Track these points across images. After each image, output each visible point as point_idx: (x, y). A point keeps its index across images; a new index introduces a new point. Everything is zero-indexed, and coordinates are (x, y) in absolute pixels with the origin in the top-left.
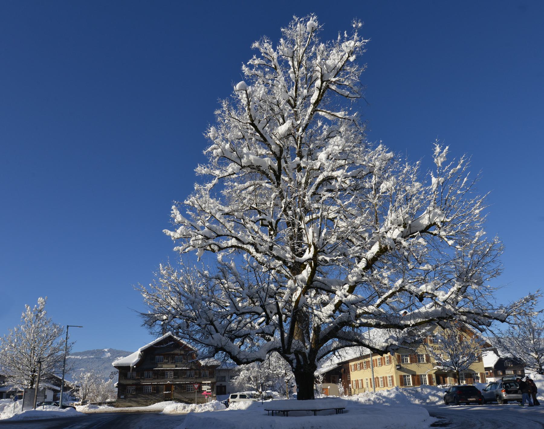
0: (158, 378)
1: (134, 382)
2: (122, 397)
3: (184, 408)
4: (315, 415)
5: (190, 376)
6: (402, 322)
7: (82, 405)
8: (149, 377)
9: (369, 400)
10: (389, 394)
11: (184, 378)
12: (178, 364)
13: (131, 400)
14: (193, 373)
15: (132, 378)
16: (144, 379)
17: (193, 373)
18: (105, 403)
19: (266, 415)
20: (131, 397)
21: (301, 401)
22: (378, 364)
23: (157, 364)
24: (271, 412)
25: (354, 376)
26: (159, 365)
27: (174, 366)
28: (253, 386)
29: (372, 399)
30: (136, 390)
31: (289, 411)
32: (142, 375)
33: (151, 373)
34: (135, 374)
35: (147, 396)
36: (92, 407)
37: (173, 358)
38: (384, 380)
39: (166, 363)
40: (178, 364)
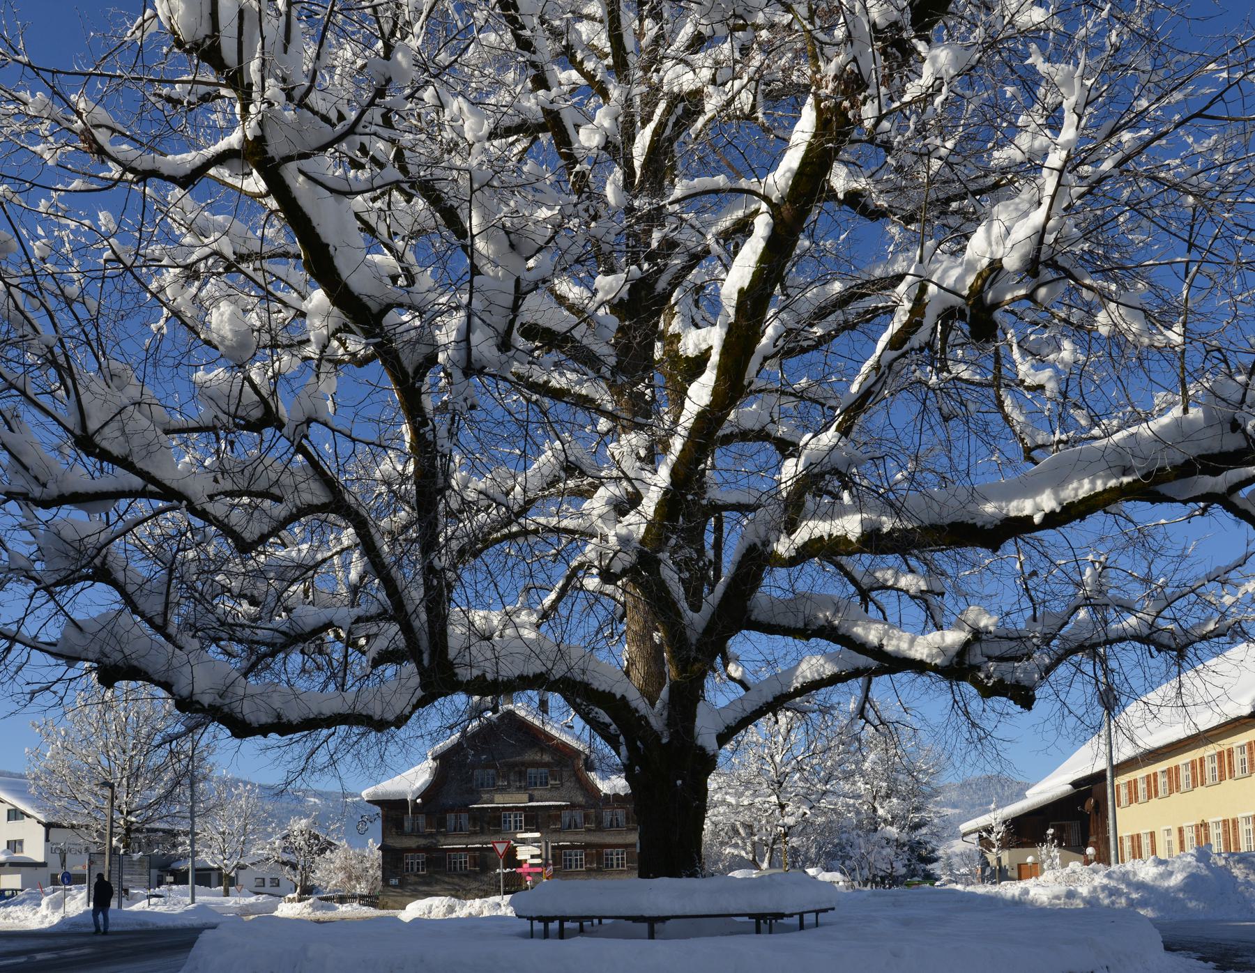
0: (482, 832)
1: (422, 842)
2: (394, 881)
3: (451, 909)
4: (652, 936)
5: (572, 826)
6: (989, 508)
7: (300, 901)
8: (458, 829)
9: (1071, 895)
10: (1163, 876)
11: (555, 831)
12: (536, 793)
13: (416, 890)
14: (578, 815)
15: (415, 832)
16: (445, 835)
17: (578, 815)
18: (353, 897)
19: (532, 935)
20: (416, 883)
21: (664, 881)
22: (1208, 774)
23: (478, 792)
24: (554, 926)
25: (1128, 820)
26: (485, 796)
27: (526, 797)
28: (743, 853)
29: (1084, 891)
30: (428, 863)
31: (664, 919)
32: (442, 823)
33: (464, 818)
34: (422, 820)
35: (456, 880)
36: (322, 908)
37: (521, 775)
38: (1226, 832)
39: (502, 790)
40: (536, 793)
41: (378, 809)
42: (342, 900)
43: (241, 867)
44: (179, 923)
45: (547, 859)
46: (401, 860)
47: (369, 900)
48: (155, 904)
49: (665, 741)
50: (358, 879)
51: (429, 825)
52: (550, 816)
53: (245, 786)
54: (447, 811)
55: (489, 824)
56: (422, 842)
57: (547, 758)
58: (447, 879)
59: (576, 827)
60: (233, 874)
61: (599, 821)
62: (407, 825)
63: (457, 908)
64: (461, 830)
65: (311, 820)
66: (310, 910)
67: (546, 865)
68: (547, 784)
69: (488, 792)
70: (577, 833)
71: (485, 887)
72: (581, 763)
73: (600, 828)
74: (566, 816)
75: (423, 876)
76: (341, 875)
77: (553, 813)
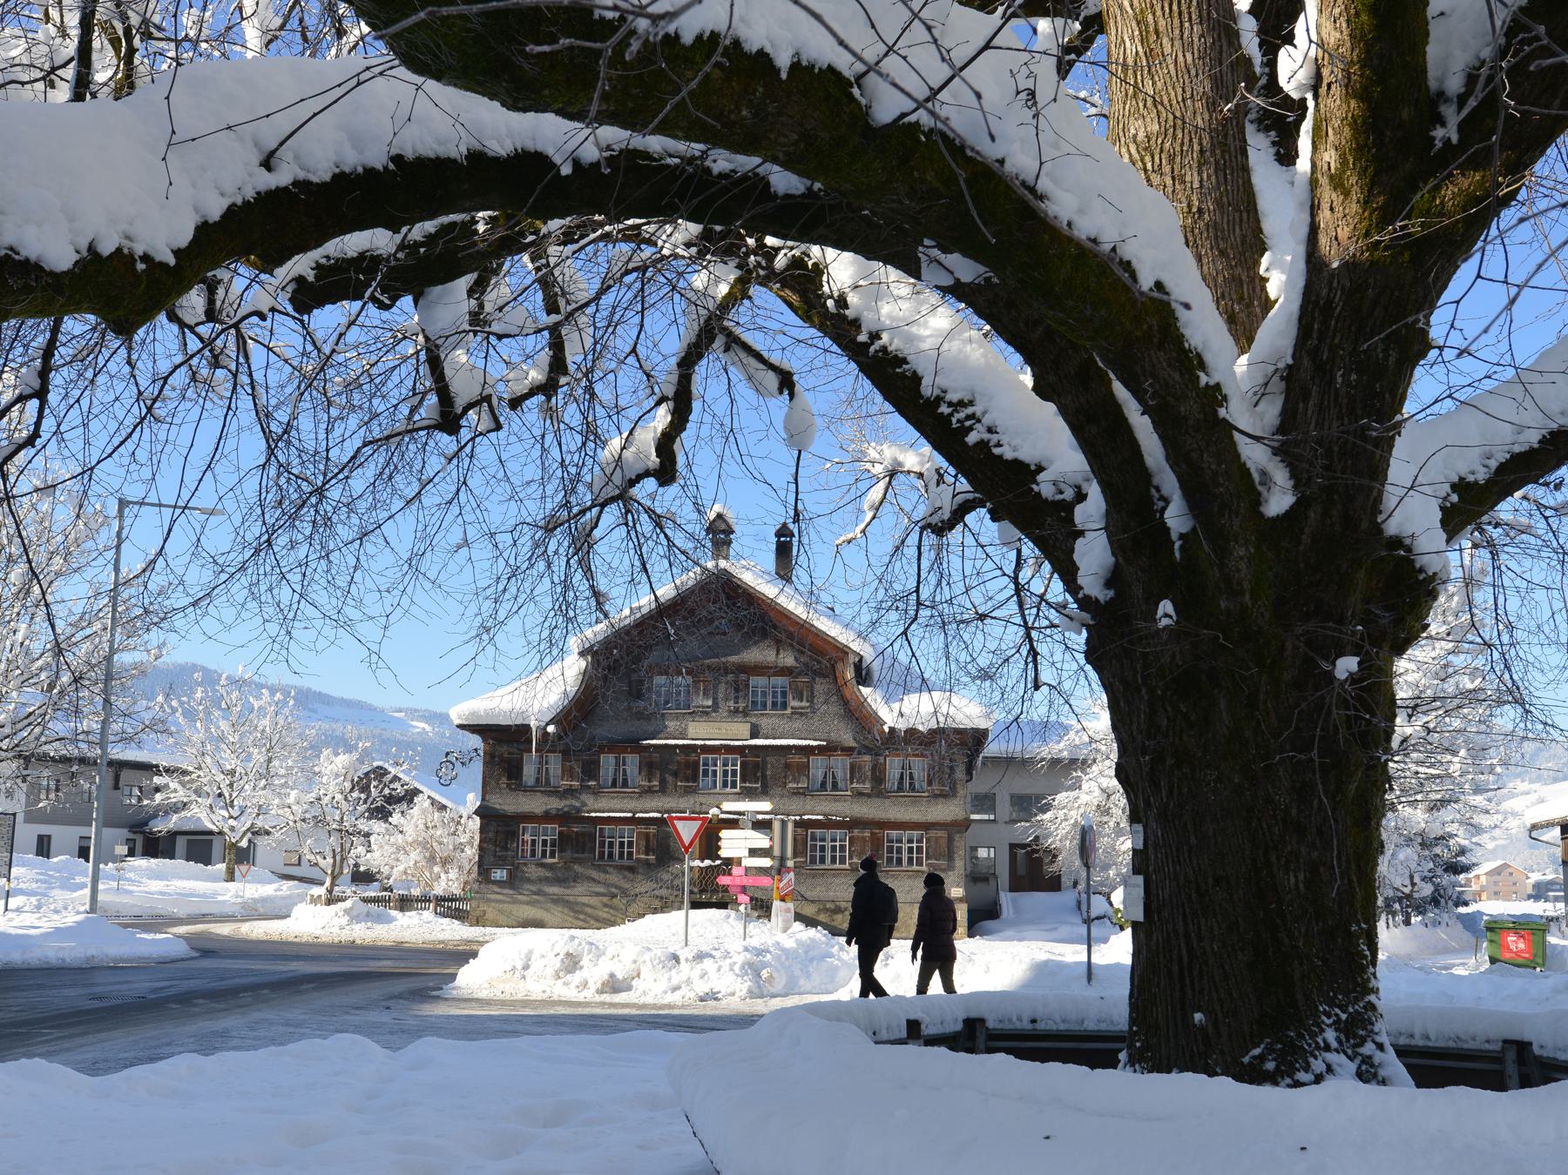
0: (663, 790)
2: (499, 874)
5: (829, 785)
7: (329, 902)
8: (620, 782)
11: (797, 793)
12: (765, 723)
14: (840, 764)
15: (542, 786)
16: (596, 793)
20: (542, 880)
27: (743, 729)
30: (563, 842)
32: (591, 770)
33: (632, 762)
34: (555, 764)
36: (368, 916)
37: (739, 689)
40: (765, 723)
41: (475, 741)
42: (405, 903)
43: (256, 832)
44: (34, 957)
45: (783, 859)
46: (514, 835)
47: (447, 906)
48: (18, 910)
49: (1278, 502)
50: (445, 862)
51: (568, 773)
52: (787, 766)
53: (273, 694)
54: (602, 750)
55: (675, 775)
56: (555, 804)
57: (788, 659)
58: (594, 874)
59: (835, 787)
60: (244, 843)
61: (878, 777)
62: (529, 772)
63: (585, 962)
64: (625, 784)
65: (355, 755)
66: (344, 920)
67: (781, 869)
68: (784, 706)
69: (677, 717)
70: (837, 799)
71: (664, 892)
72: (850, 674)
73: (879, 789)
74: (818, 766)
75: (551, 867)
76: (415, 855)
77: (797, 759)
